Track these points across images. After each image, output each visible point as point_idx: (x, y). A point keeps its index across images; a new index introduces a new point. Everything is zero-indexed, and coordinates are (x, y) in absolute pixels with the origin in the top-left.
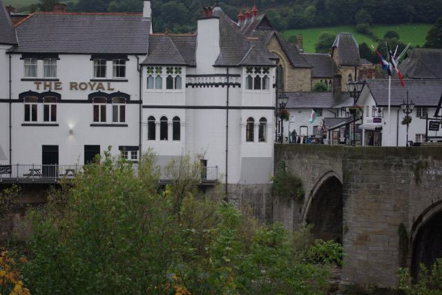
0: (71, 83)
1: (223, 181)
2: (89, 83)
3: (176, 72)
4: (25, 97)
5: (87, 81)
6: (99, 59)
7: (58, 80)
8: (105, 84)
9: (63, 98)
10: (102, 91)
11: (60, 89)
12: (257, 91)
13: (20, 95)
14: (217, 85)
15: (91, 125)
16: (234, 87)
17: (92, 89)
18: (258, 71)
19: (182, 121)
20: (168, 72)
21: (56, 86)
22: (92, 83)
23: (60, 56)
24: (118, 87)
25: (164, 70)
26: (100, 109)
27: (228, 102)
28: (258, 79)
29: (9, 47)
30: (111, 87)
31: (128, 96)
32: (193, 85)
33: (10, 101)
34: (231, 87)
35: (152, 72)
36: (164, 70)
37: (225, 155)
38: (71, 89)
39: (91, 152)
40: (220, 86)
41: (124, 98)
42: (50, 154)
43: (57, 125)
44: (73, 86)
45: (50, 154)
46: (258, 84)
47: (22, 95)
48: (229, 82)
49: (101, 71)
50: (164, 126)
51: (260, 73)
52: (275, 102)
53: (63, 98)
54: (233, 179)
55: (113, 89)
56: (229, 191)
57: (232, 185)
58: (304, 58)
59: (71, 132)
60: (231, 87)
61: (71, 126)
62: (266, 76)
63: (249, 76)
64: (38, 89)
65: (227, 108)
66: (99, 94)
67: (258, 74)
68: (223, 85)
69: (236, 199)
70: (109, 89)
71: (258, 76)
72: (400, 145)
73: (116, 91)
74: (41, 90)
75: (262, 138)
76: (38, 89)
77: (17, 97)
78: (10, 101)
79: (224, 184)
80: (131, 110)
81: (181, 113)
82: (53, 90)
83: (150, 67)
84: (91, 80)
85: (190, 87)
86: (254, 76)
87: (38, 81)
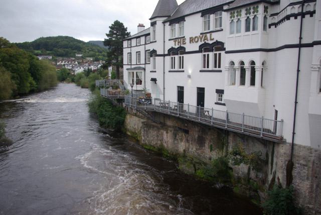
0: (191, 38)
1: (289, 140)
2: (200, 36)
4: (172, 51)
8: (208, 35)
9: (187, 50)
10: (207, 42)
11: (185, 44)
13: (168, 51)
14: (288, 18)
15: (201, 71)
16: (296, 18)
17: (201, 41)
19: (258, 65)
20: (246, 14)
21: (183, 42)
22: (201, 36)
23: (186, 18)
24: (217, 37)
25: (243, 12)
26: (218, 54)
27: (301, 38)
30: (212, 38)
31: (222, 44)
32: (276, 25)
33: (164, 55)
34: (307, 16)
36: (243, 12)
37: (165, 86)
38: (190, 43)
39: (201, 93)
40: (292, 18)
41: (219, 46)
42: (181, 92)
43: (183, 71)
44: (192, 40)
45: (181, 92)
47: (169, 50)
48: (304, 11)
49: (207, 24)
50: (243, 71)
52: (299, 41)
53: (187, 50)
54: (303, 139)
55: (213, 39)
56: (296, 152)
57: (300, 146)
59: (189, 77)
60: (307, 16)
61: (190, 72)
62: (255, 16)
64: (175, 45)
65: (300, 46)
66: (205, 44)
68: (295, 16)
69: (304, 165)
70: (211, 39)
73: (215, 41)
75: (253, 83)
76: (175, 45)
77: (166, 53)
78: (164, 55)
79: (290, 144)
80: (226, 59)
81: (257, 57)
82: (182, 46)
83: (233, 12)
84: (201, 34)
85: (273, 27)
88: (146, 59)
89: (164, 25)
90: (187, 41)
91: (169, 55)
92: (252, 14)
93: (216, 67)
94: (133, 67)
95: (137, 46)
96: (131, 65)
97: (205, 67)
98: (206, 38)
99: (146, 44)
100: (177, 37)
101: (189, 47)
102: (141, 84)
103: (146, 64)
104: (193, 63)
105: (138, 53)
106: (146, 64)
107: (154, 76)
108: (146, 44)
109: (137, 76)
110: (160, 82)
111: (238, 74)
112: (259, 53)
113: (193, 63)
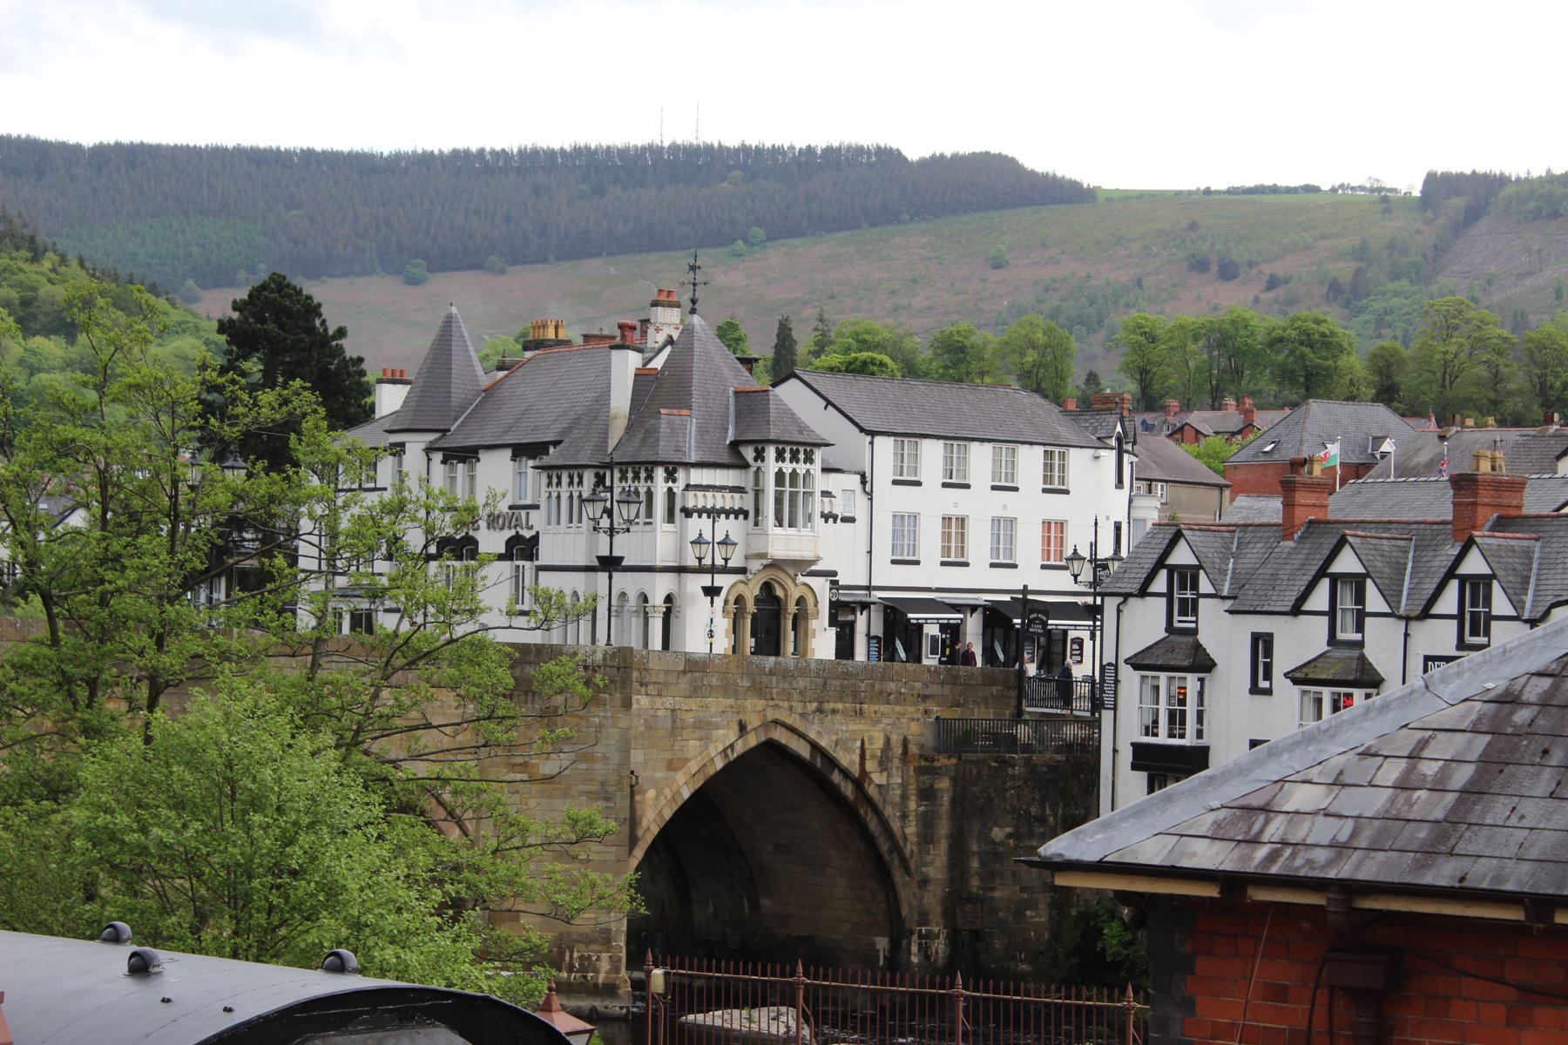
3: (646, 479)
23: (483, 455)
29: (432, 437)
63: (670, 489)
89: (429, 460)
112: (582, 575)
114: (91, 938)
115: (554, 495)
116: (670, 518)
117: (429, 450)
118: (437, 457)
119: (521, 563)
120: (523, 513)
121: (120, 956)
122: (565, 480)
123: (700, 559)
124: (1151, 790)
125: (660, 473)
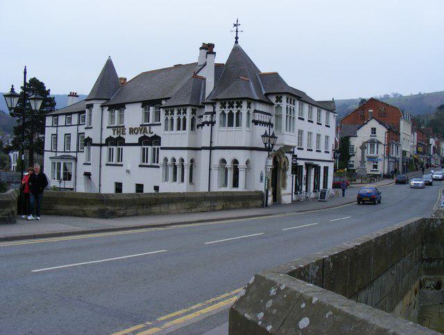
0: (130, 129)
4: (111, 141)
5: (138, 126)
6: (146, 104)
7: (124, 126)
12: (230, 128)
15: (140, 166)
16: (208, 125)
18: (231, 106)
19: (242, 164)
23: (126, 106)
27: (211, 142)
28: (231, 114)
29: (103, 102)
33: (101, 145)
35: (225, 108)
40: (206, 125)
41: (157, 140)
42: (119, 187)
44: (132, 131)
45: (119, 187)
46: (232, 121)
47: (107, 140)
51: (233, 108)
58: (41, 112)
62: (239, 111)
67: (231, 109)
71: (231, 111)
72: (103, 192)
74: (115, 136)
77: (104, 142)
78: (101, 145)
81: (242, 156)
82: (122, 136)
85: (200, 128)
86: (227, 111)
87: (114, 128)
88: (78, 145)
90: (127, 131)
91: (106, 145)
92: (235, 108)
93: (144, 162)
94: (59, 154)
95: (66, 126)
96: (56, 152)
97: (144, 162)
98: (145, 131)
99: (79, 124)
100: (116, 125)
101: (130, 138)
102: (70, 179)
103: (78, 151)
104: (132, 155)
105: (68, 136)
106: (78, 151)
107: (88, 169)
108: (79, 124)
109: (65, 169)
110: (94, 177)
111: (171, 170)
112: (187, 151)
113: (132, 155)
114: (370, 109)
115: (169, 118)
116: (248, 125)
117: (102, 106)
118: (106, 109)
119: (146, 147)
120: (148, 128)
121: (161, 191)
122: (176, 112)
123: (266, 144)
124: (109, 66)
125: (245, 104)
